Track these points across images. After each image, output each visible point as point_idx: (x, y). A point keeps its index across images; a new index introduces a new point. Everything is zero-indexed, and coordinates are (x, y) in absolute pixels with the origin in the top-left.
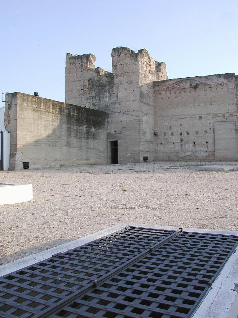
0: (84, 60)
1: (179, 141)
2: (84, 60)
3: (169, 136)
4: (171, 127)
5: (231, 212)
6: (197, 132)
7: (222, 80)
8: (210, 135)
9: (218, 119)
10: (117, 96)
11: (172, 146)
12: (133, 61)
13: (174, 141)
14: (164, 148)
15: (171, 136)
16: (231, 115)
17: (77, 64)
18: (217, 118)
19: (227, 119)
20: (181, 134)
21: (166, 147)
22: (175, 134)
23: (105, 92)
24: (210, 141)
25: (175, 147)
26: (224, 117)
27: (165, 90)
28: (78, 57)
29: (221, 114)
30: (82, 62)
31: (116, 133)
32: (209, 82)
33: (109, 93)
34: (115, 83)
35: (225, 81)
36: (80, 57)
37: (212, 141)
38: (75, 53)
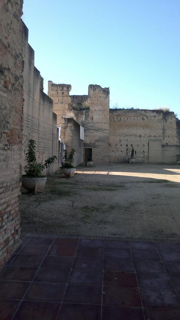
0: (65, 89)
1: (125, 150)
2: (65, 89)
3: (118, 146)
4: (120, 141)
5: (46, 216)
6: (138, 146)
7: (155, 114)
8: (146, 147)
9: (151, 138)
10: (92, 118)
11: (121, 153)
12: (105, 96)
13: (122, 150)
14: (115, 154)
15: (120, 147)
16: (160, 136)
17: (59, 91)
18: (151, 137)
19: (157, 138)
20: (127, 145)
21: (117, 153)
22: (123, 145)
23: (83, 114)
24: (146, 150)
25: (122, 154)
26: (155, 137)
27: (116, 116)
28: (60, 85)
29: (153, 134)
30: (63, 89)
31: (91, 143)
32: (147, 114)
33: (85, 115)
34: (90, 109)
35: (157, 115)
36: (62, 86)
37: (147, 151)
38: (57, 82)
